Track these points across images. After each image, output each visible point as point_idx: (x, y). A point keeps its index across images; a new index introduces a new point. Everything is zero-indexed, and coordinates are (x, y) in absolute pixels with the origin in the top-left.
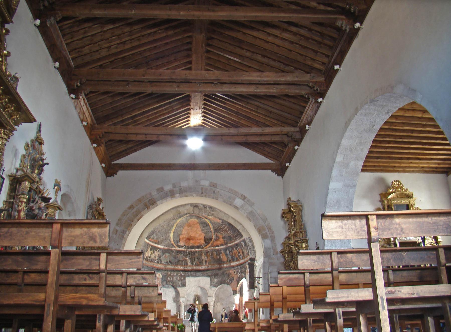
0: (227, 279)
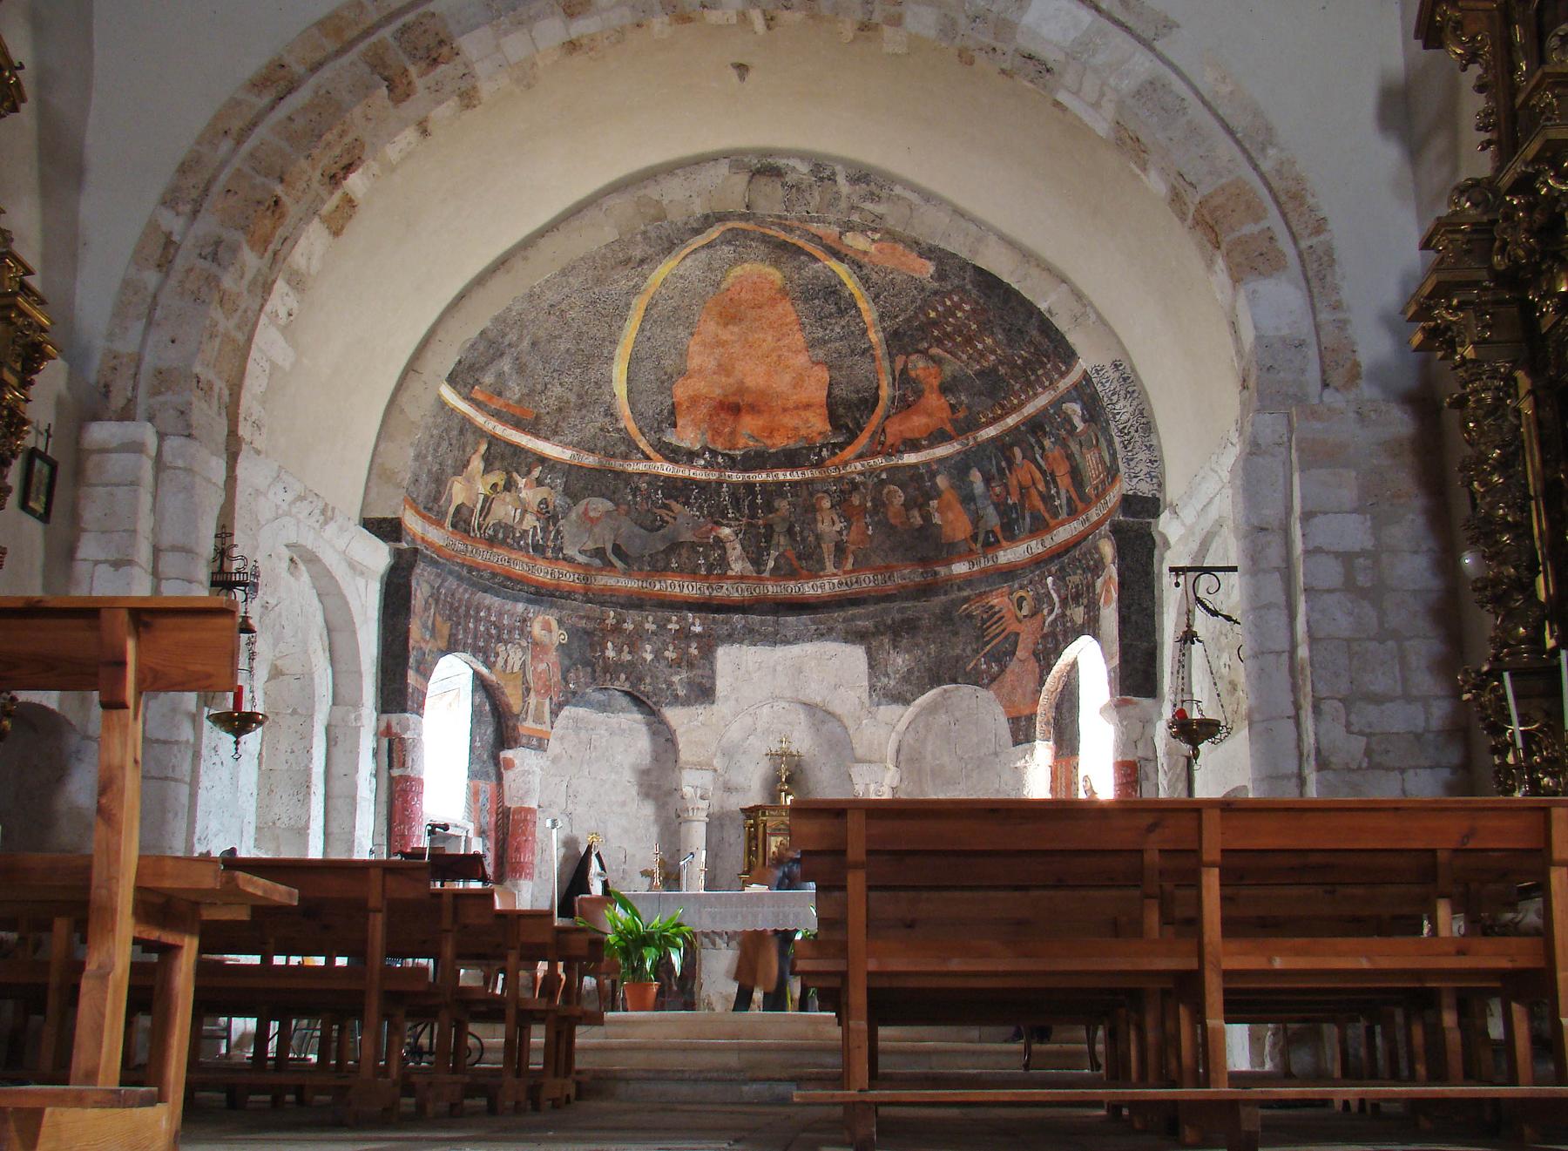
0: (976, 652)
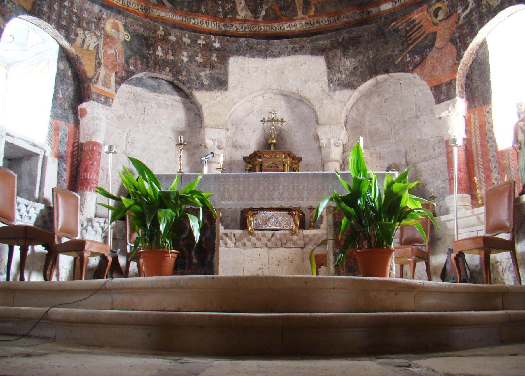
0: (403, 51)
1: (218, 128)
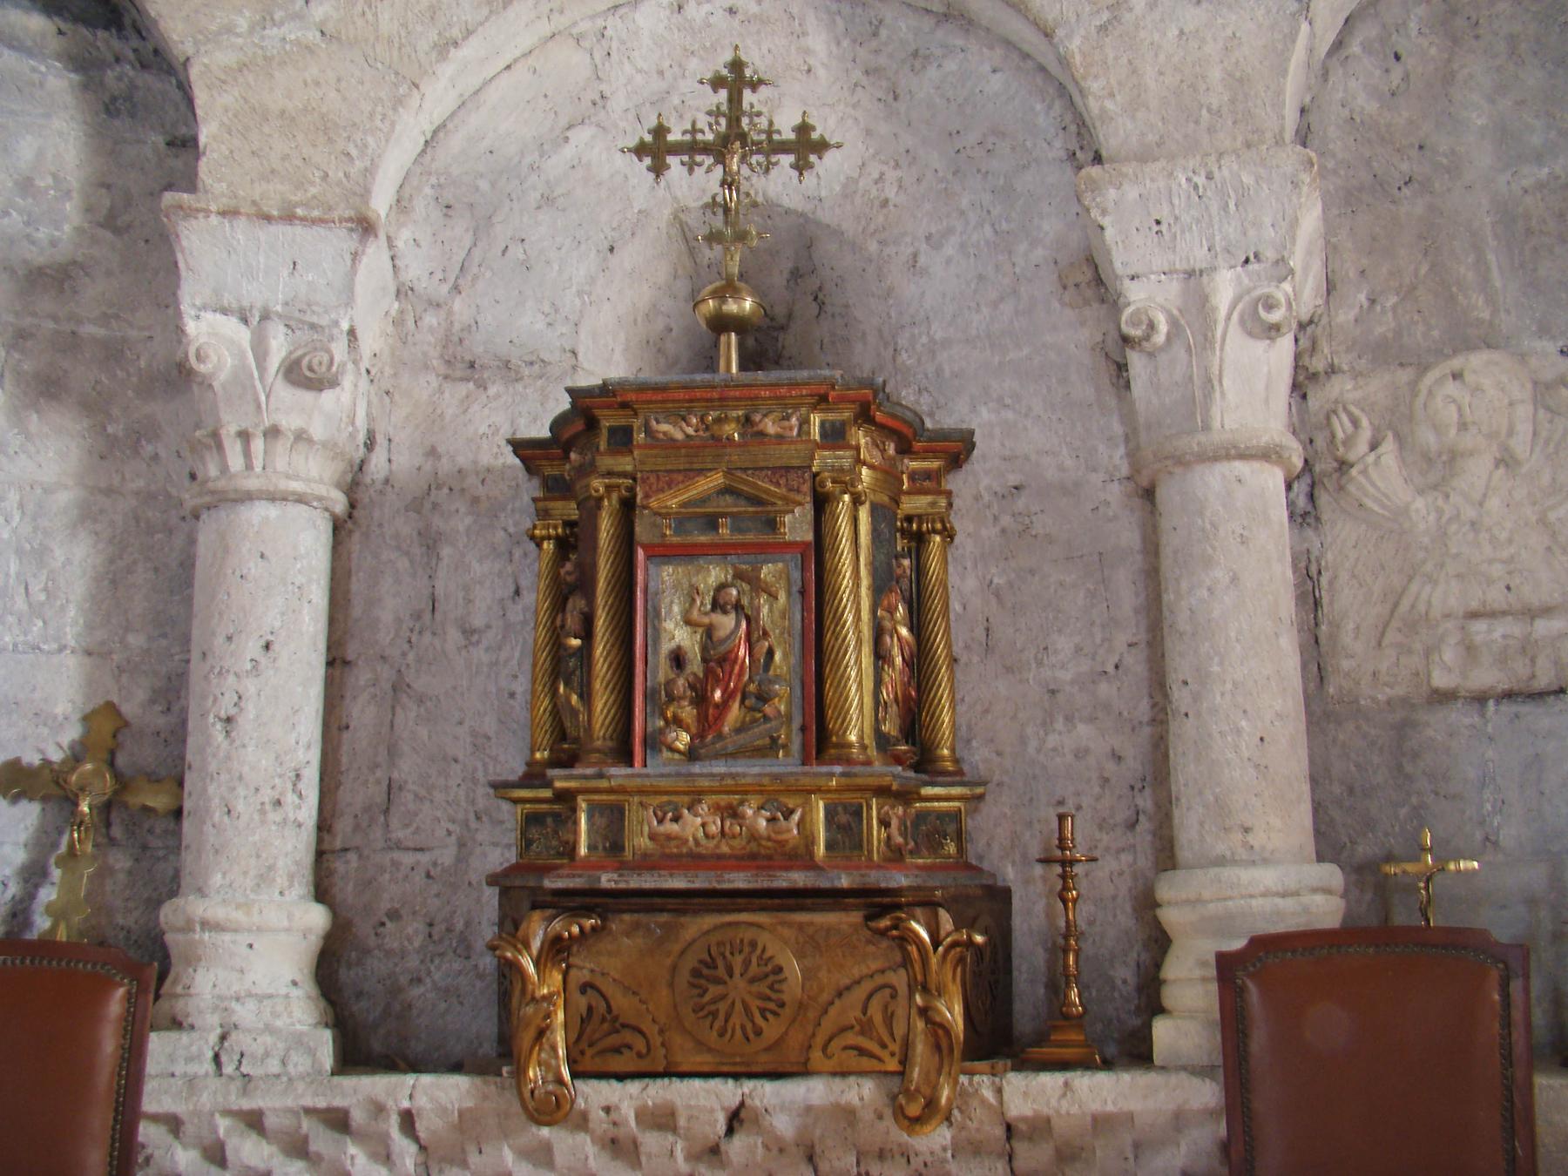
1: (289, 218)
